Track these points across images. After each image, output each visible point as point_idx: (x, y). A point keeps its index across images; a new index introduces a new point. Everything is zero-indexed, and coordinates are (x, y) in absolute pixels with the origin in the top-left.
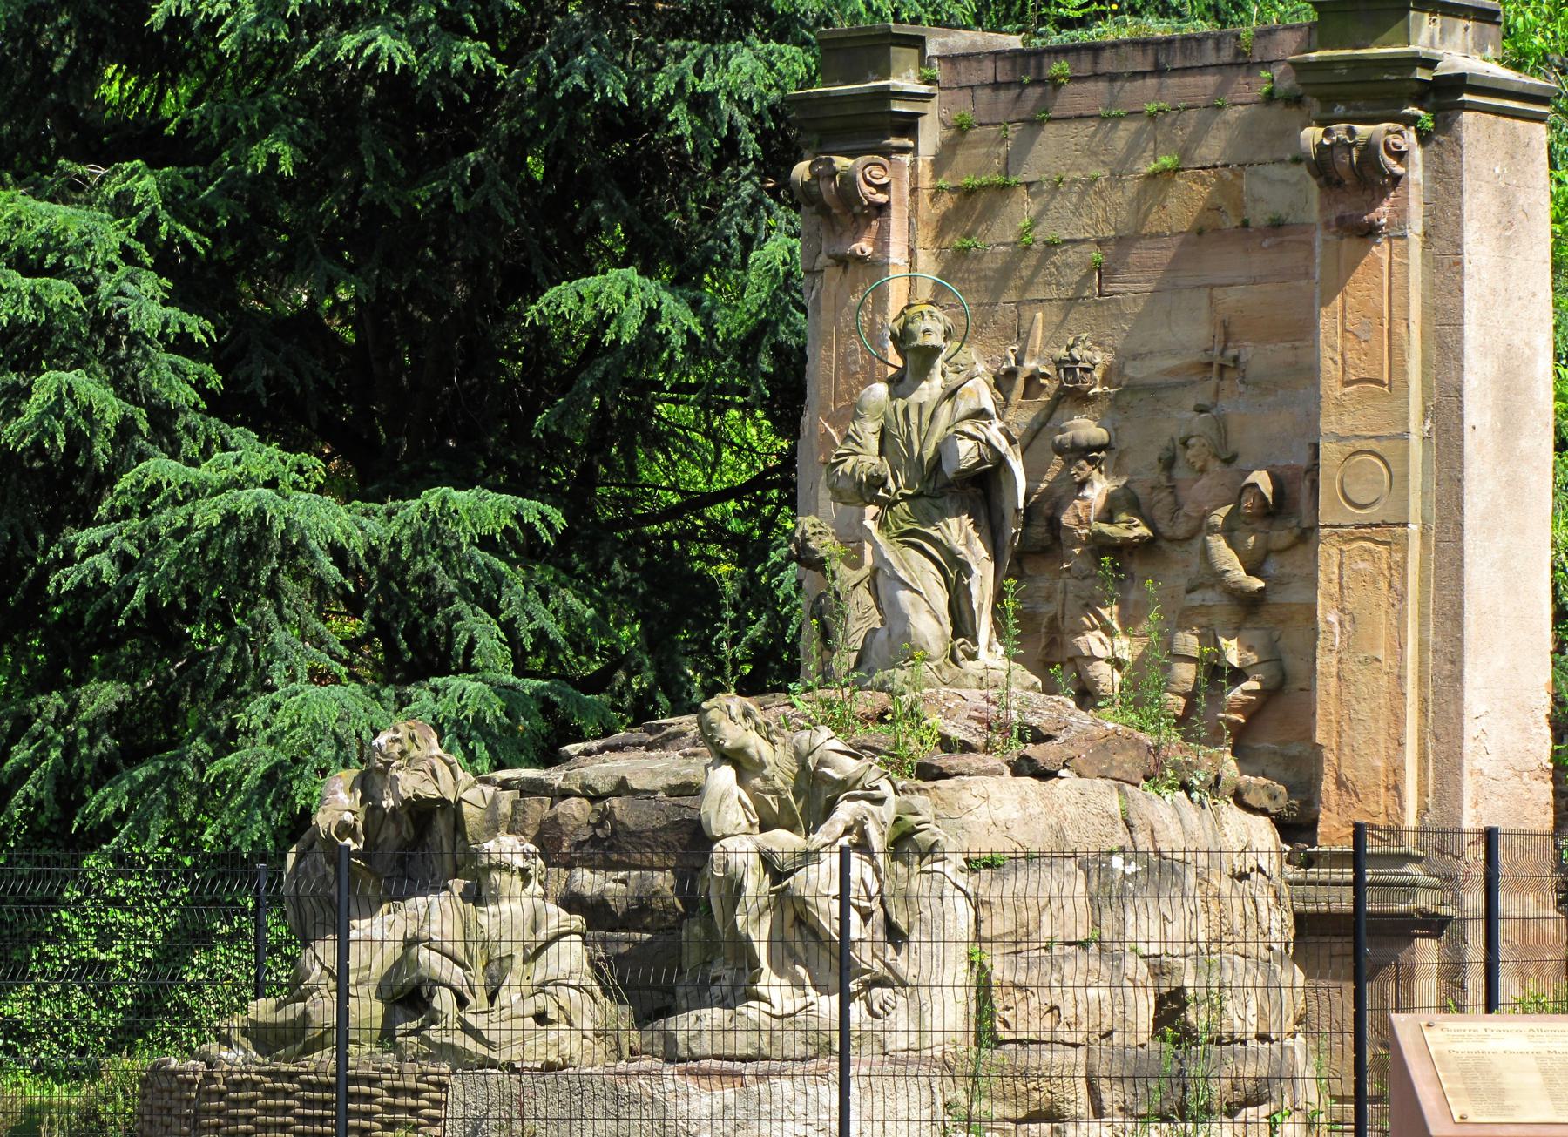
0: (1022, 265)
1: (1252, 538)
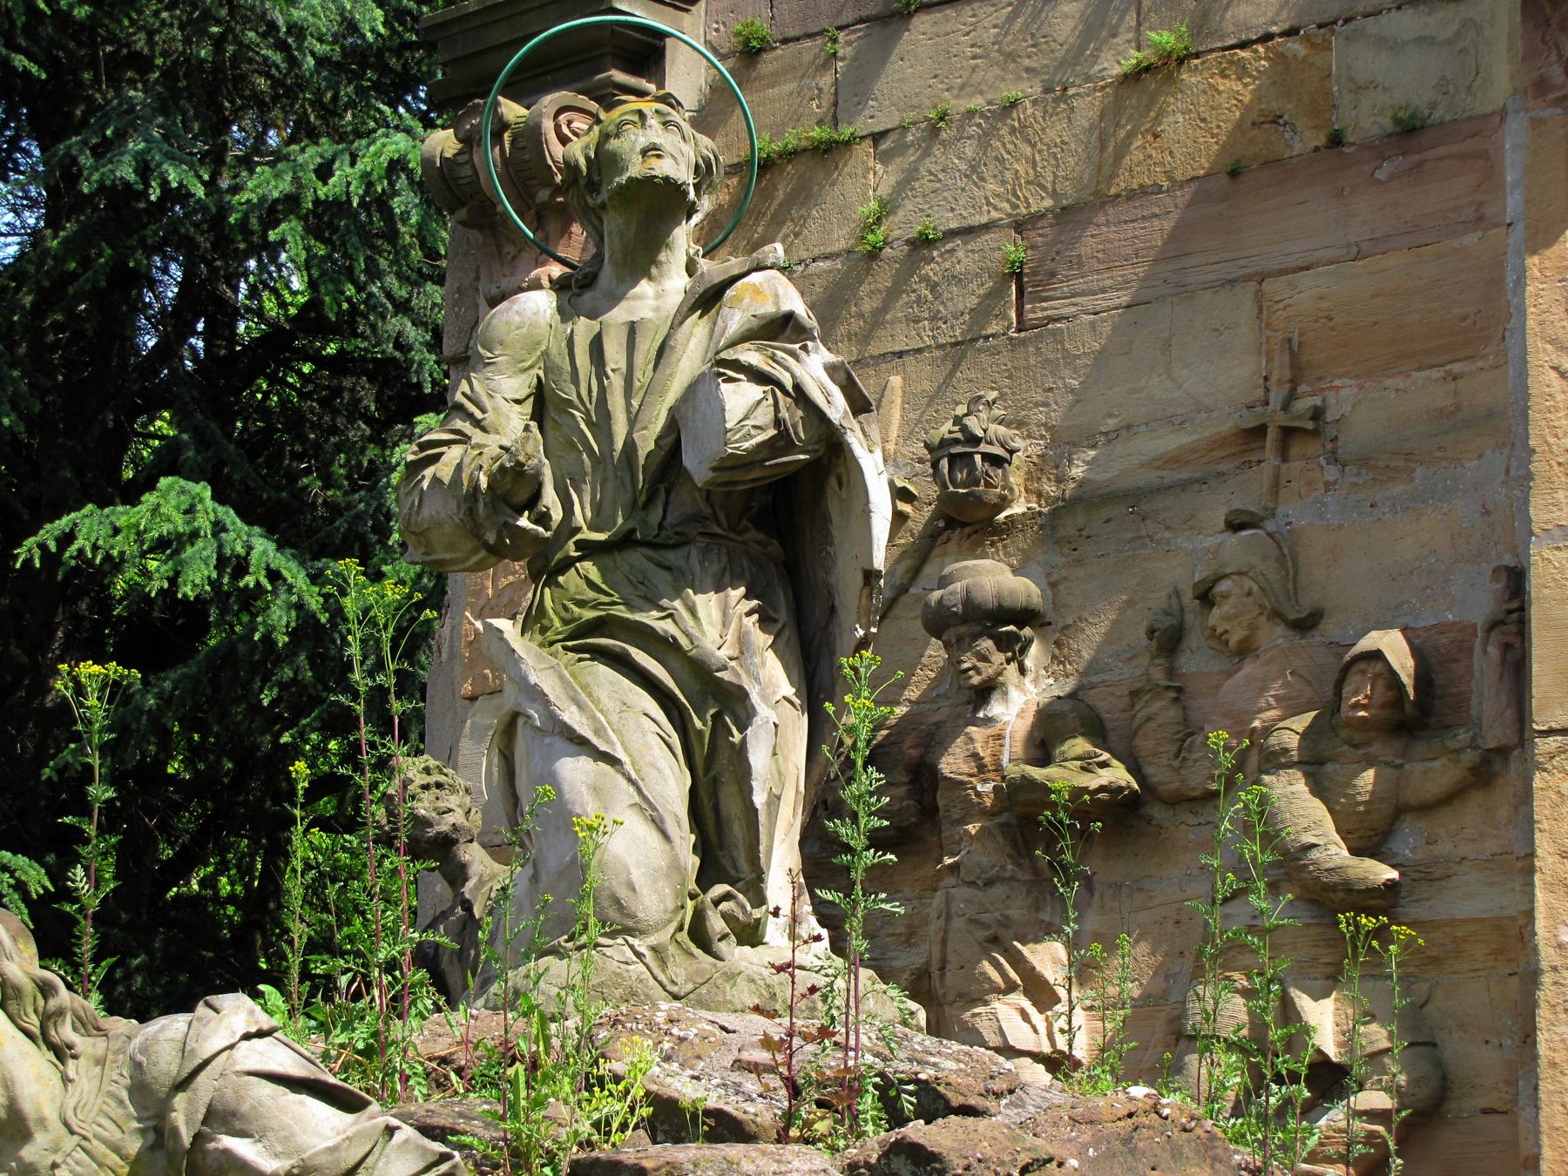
0: (864, 289)
1: (1369, 775)
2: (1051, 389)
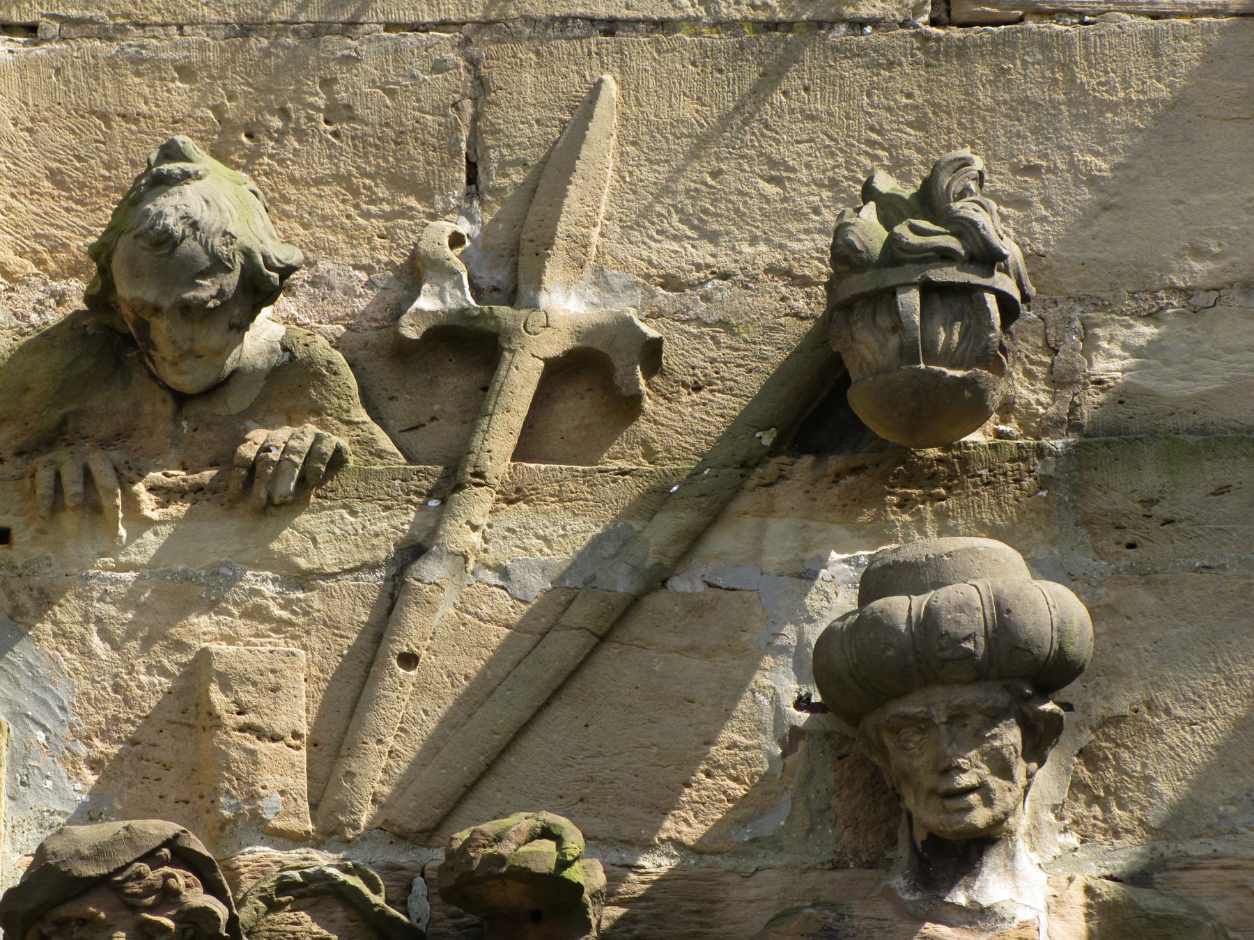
2: (1032, 170)
